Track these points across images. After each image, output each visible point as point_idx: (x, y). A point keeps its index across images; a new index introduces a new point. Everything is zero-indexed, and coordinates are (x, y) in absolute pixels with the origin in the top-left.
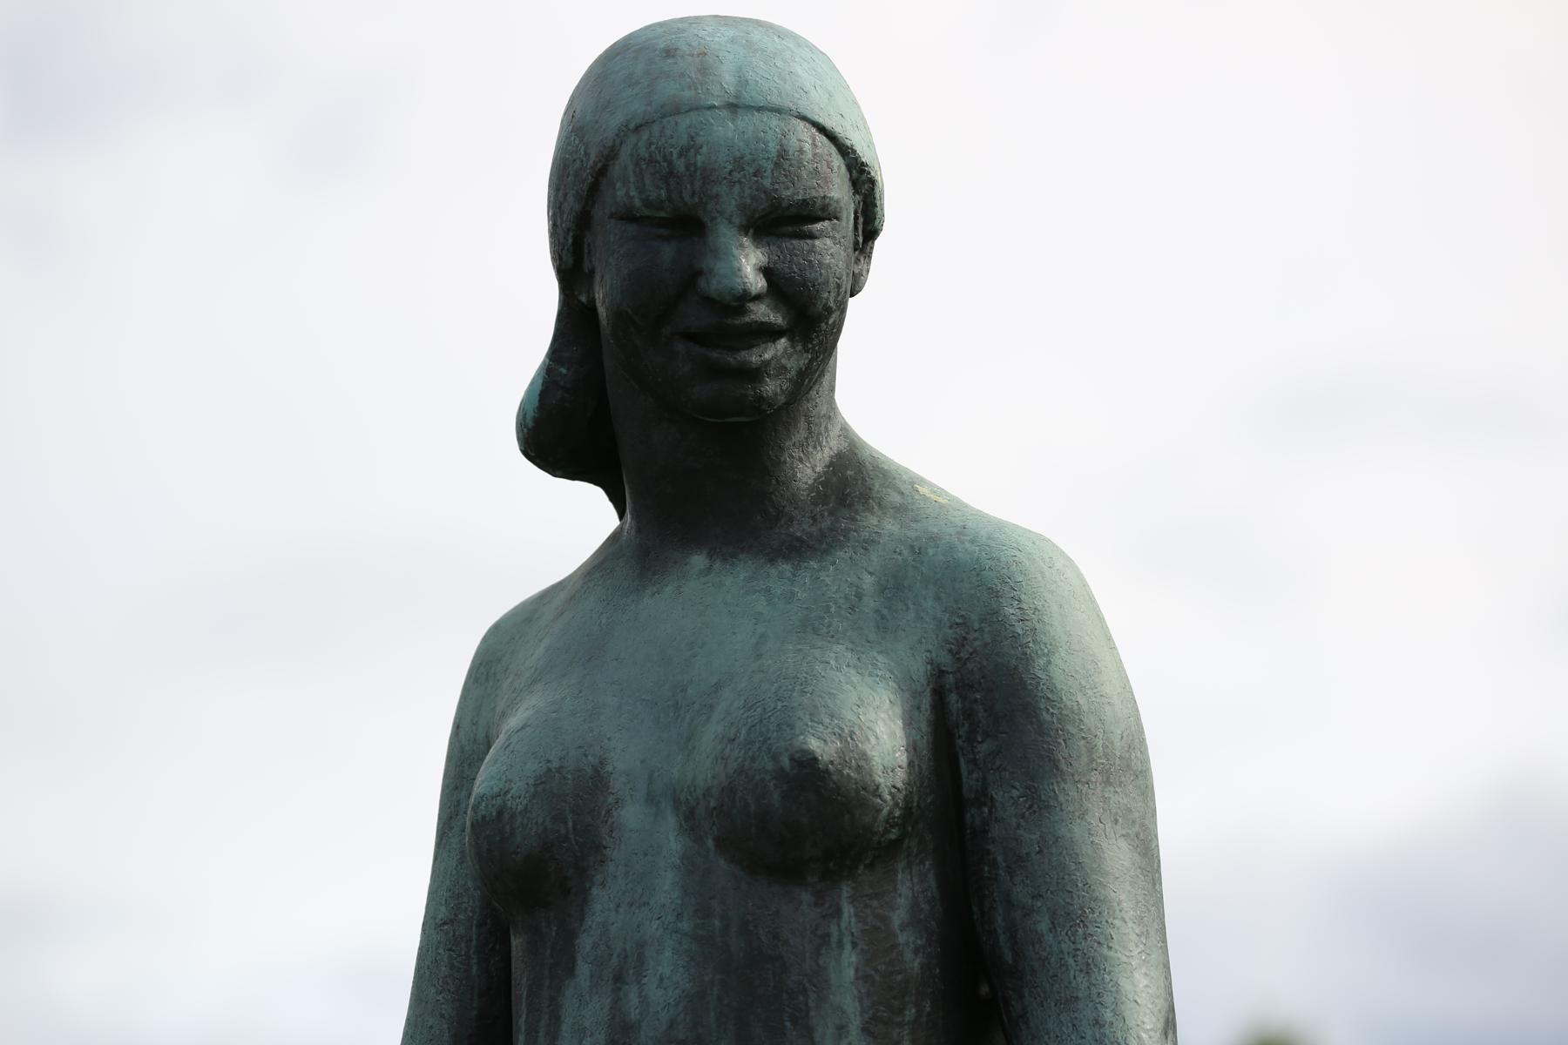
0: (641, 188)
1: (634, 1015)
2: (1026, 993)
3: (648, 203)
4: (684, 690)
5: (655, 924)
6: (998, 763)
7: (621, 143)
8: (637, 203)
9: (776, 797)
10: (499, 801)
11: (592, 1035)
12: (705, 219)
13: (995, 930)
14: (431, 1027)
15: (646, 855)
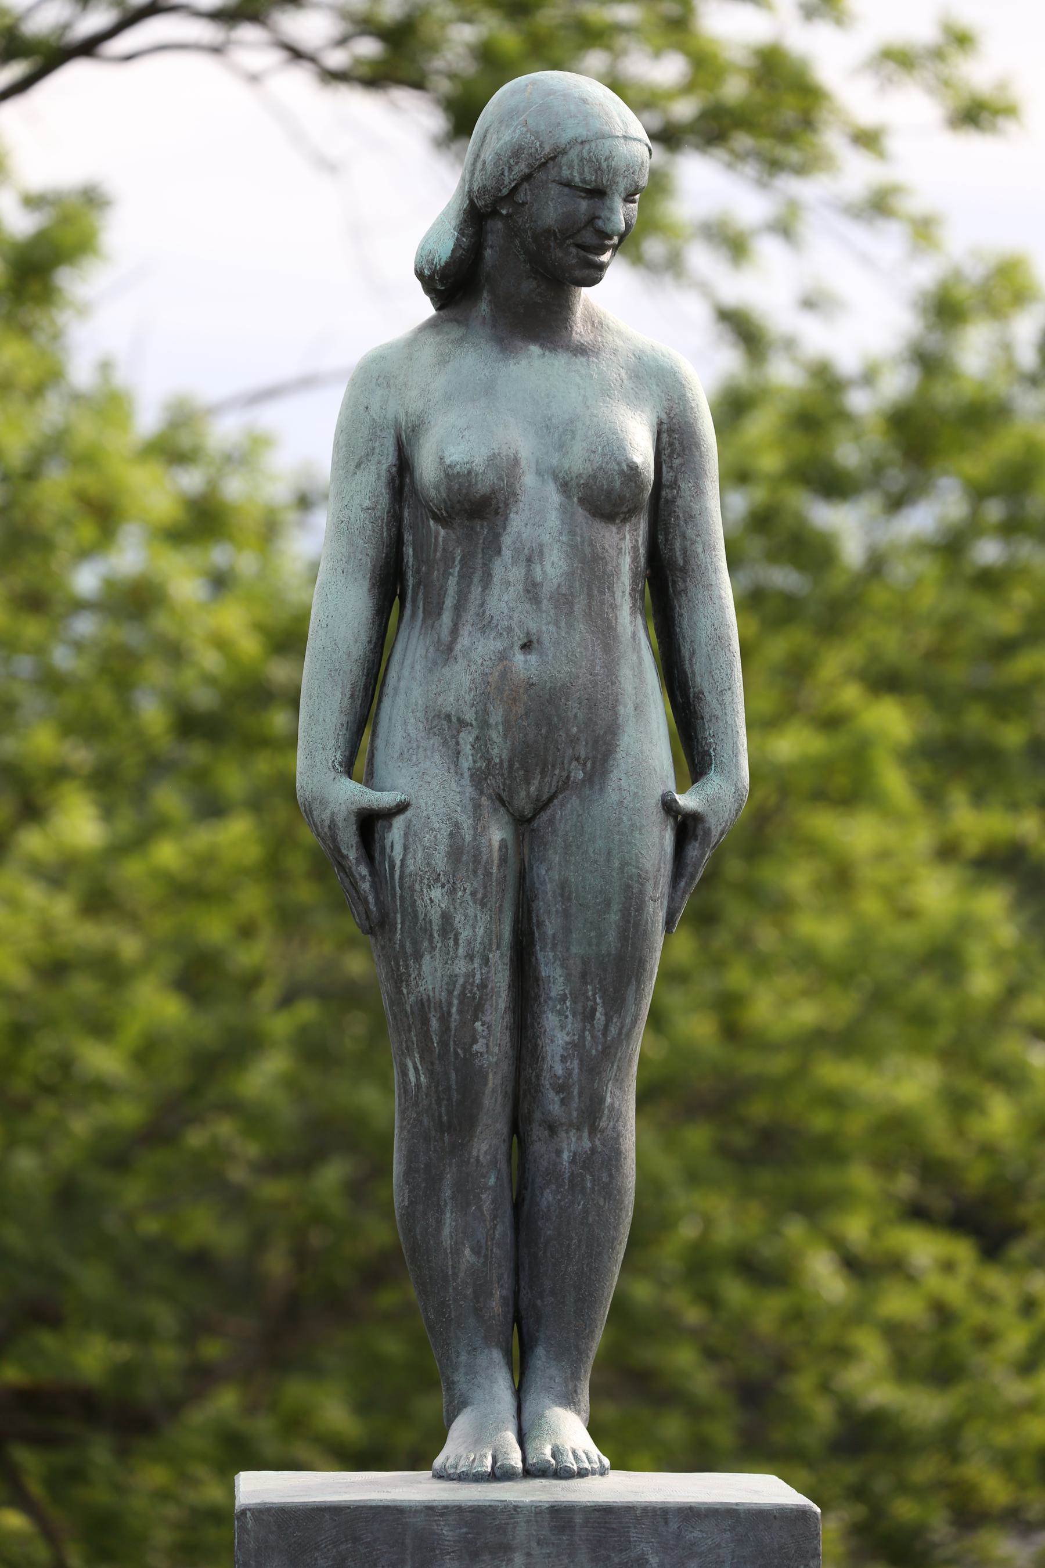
0: (582, 173)
1: (539, 579)
2: (688, 579)
3: (584, 181)
4: (550, 419)
5: (548, 536)
6: (683, 469)
7: (571, 148)
8: (577, 179)
9: (618, 484)
10: (468, 466)
11: (514, 585)
12: (610, 193)
13: (674, 549)
14: (361, 559)
15: (540, 501)
